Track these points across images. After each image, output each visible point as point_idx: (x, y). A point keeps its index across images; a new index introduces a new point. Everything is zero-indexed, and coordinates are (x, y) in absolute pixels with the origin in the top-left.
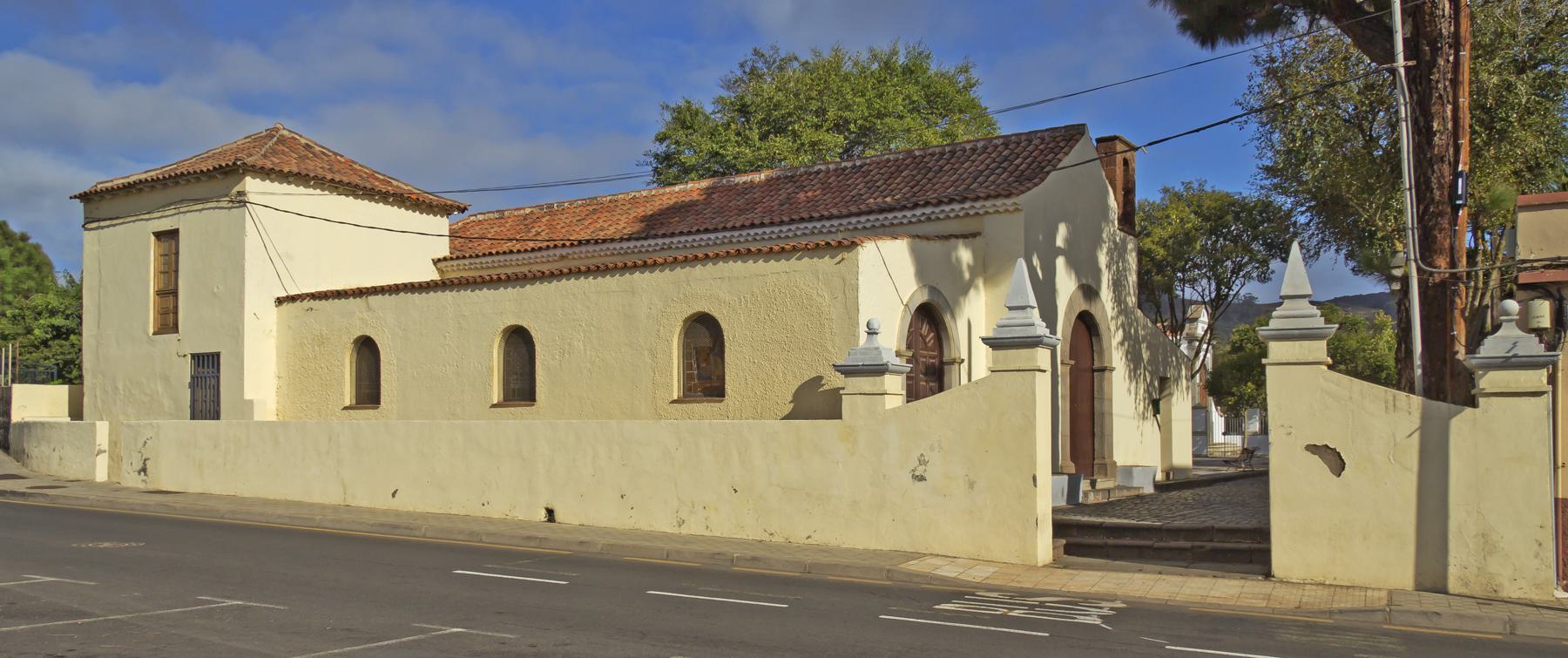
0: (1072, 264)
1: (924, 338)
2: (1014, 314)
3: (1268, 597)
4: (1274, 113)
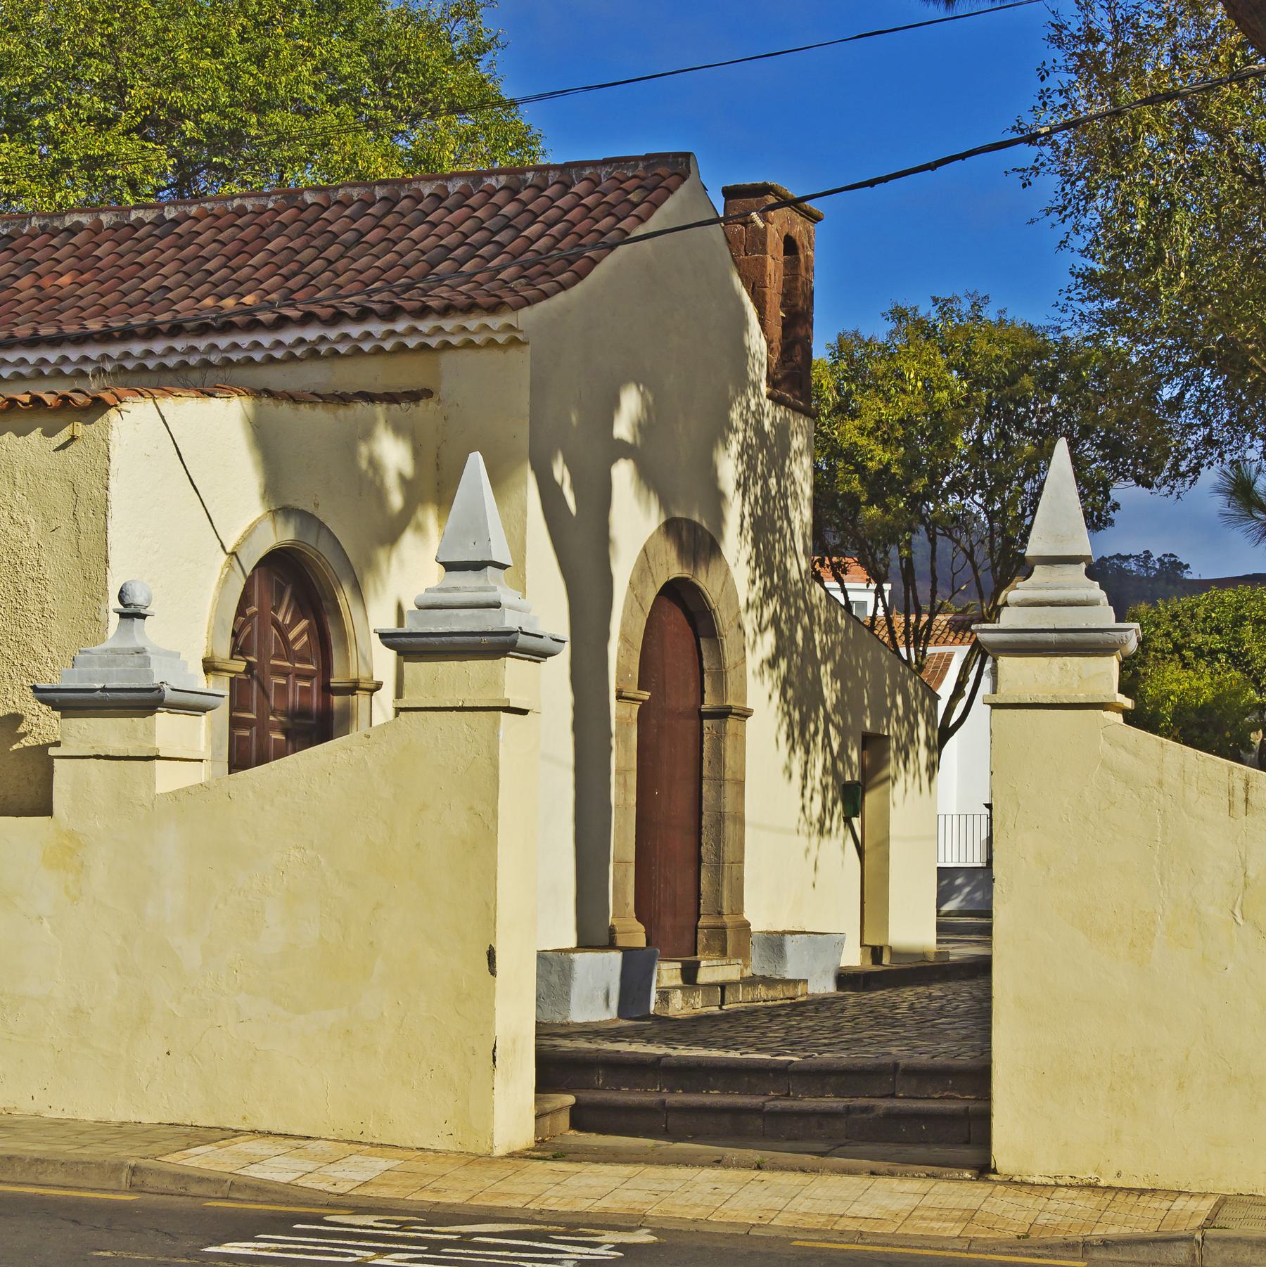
0: (648, 478)
1: (283, 631)
2: (458, 578)
3: (970, 1216)
4: (1105, 149)
